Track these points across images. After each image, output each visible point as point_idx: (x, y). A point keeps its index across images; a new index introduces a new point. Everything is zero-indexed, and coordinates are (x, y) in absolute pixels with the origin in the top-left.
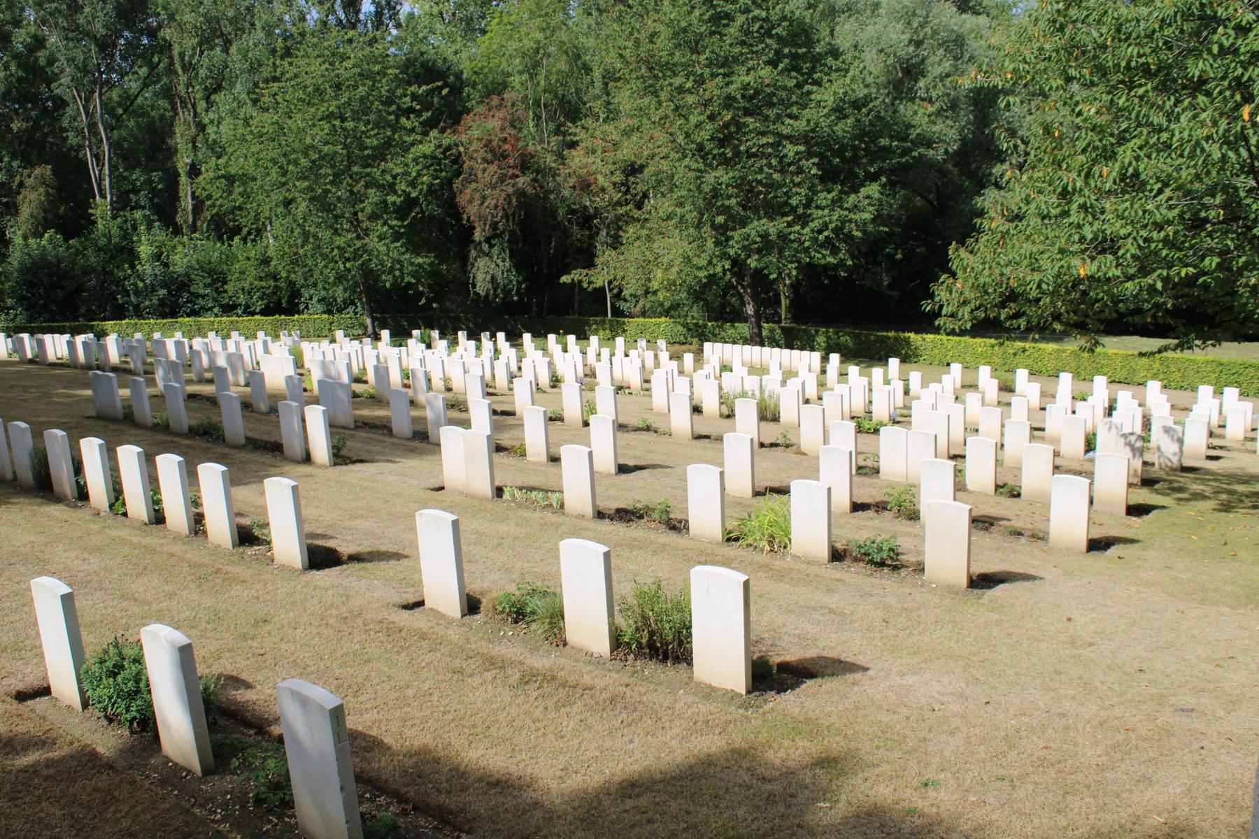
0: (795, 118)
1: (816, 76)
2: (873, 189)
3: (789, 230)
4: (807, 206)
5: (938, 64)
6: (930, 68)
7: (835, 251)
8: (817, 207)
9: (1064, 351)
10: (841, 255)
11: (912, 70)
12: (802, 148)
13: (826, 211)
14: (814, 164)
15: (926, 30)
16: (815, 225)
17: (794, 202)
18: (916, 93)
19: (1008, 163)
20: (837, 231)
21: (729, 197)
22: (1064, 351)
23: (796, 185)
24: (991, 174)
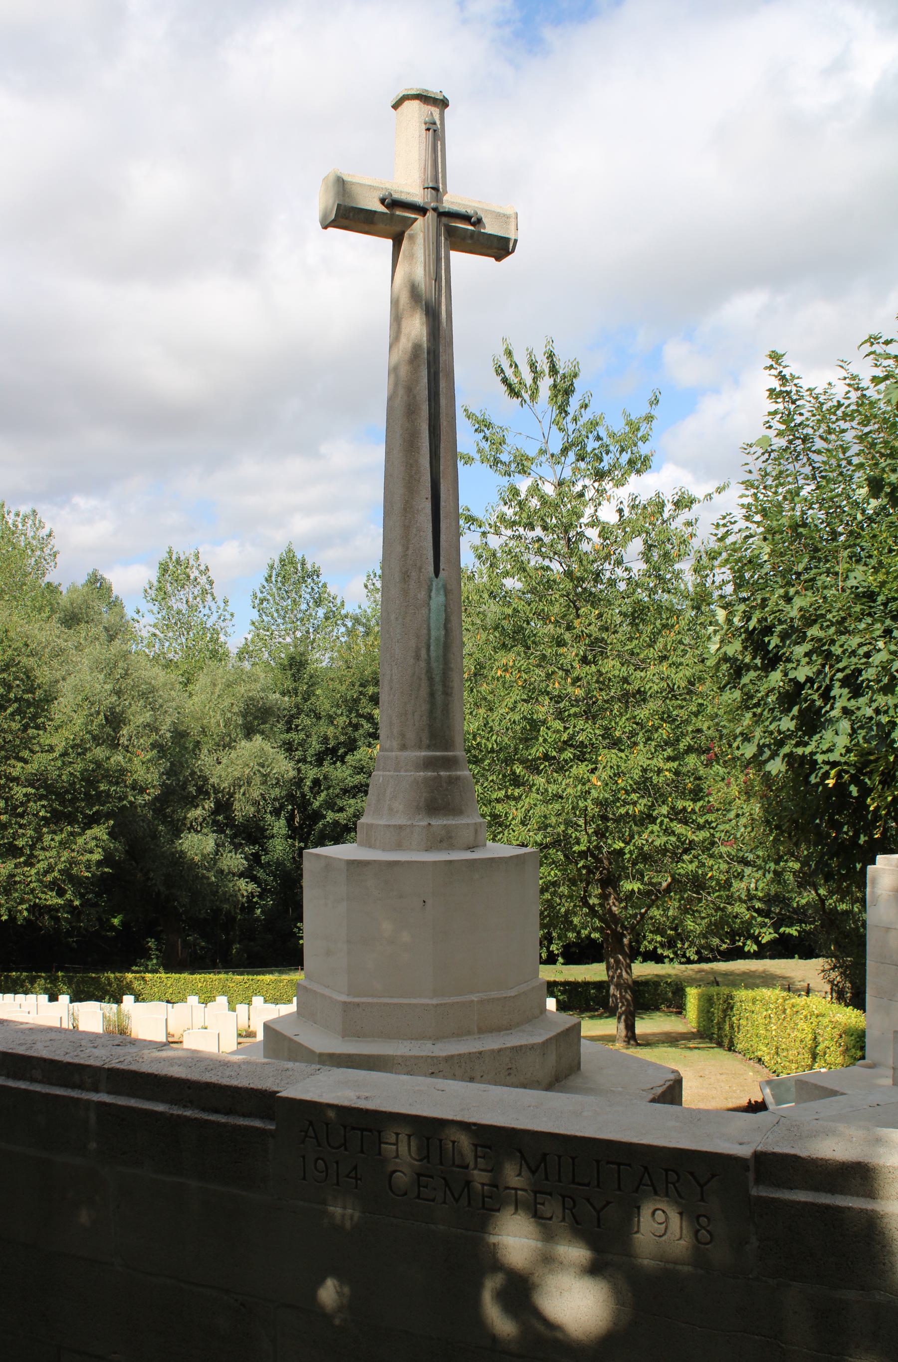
0: (26, 762)
1: (39, 721)
2: (100, 831)
3: (19, 871)
4: (33, 847)
5: (139, 716)
6: (132, 717)
7: (61, 893)
8: (43, 849)
9: (281, 981)
10: (68, 896)
11: (115, 720)
12: (31, 790)
13: (54, 853)
14: (43, 806)
15: (129, 681)
16: (42, 866)
17: (20, 843)
18: (119, 740)
19: (200, 808)
20: (65, 872)
21: (720, 746)
22: (281, 981)
23: (21, 826)
24: (185, 818)
